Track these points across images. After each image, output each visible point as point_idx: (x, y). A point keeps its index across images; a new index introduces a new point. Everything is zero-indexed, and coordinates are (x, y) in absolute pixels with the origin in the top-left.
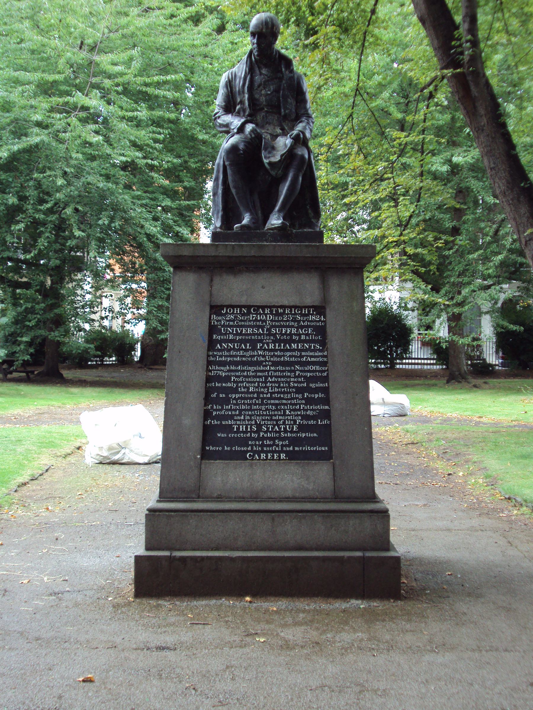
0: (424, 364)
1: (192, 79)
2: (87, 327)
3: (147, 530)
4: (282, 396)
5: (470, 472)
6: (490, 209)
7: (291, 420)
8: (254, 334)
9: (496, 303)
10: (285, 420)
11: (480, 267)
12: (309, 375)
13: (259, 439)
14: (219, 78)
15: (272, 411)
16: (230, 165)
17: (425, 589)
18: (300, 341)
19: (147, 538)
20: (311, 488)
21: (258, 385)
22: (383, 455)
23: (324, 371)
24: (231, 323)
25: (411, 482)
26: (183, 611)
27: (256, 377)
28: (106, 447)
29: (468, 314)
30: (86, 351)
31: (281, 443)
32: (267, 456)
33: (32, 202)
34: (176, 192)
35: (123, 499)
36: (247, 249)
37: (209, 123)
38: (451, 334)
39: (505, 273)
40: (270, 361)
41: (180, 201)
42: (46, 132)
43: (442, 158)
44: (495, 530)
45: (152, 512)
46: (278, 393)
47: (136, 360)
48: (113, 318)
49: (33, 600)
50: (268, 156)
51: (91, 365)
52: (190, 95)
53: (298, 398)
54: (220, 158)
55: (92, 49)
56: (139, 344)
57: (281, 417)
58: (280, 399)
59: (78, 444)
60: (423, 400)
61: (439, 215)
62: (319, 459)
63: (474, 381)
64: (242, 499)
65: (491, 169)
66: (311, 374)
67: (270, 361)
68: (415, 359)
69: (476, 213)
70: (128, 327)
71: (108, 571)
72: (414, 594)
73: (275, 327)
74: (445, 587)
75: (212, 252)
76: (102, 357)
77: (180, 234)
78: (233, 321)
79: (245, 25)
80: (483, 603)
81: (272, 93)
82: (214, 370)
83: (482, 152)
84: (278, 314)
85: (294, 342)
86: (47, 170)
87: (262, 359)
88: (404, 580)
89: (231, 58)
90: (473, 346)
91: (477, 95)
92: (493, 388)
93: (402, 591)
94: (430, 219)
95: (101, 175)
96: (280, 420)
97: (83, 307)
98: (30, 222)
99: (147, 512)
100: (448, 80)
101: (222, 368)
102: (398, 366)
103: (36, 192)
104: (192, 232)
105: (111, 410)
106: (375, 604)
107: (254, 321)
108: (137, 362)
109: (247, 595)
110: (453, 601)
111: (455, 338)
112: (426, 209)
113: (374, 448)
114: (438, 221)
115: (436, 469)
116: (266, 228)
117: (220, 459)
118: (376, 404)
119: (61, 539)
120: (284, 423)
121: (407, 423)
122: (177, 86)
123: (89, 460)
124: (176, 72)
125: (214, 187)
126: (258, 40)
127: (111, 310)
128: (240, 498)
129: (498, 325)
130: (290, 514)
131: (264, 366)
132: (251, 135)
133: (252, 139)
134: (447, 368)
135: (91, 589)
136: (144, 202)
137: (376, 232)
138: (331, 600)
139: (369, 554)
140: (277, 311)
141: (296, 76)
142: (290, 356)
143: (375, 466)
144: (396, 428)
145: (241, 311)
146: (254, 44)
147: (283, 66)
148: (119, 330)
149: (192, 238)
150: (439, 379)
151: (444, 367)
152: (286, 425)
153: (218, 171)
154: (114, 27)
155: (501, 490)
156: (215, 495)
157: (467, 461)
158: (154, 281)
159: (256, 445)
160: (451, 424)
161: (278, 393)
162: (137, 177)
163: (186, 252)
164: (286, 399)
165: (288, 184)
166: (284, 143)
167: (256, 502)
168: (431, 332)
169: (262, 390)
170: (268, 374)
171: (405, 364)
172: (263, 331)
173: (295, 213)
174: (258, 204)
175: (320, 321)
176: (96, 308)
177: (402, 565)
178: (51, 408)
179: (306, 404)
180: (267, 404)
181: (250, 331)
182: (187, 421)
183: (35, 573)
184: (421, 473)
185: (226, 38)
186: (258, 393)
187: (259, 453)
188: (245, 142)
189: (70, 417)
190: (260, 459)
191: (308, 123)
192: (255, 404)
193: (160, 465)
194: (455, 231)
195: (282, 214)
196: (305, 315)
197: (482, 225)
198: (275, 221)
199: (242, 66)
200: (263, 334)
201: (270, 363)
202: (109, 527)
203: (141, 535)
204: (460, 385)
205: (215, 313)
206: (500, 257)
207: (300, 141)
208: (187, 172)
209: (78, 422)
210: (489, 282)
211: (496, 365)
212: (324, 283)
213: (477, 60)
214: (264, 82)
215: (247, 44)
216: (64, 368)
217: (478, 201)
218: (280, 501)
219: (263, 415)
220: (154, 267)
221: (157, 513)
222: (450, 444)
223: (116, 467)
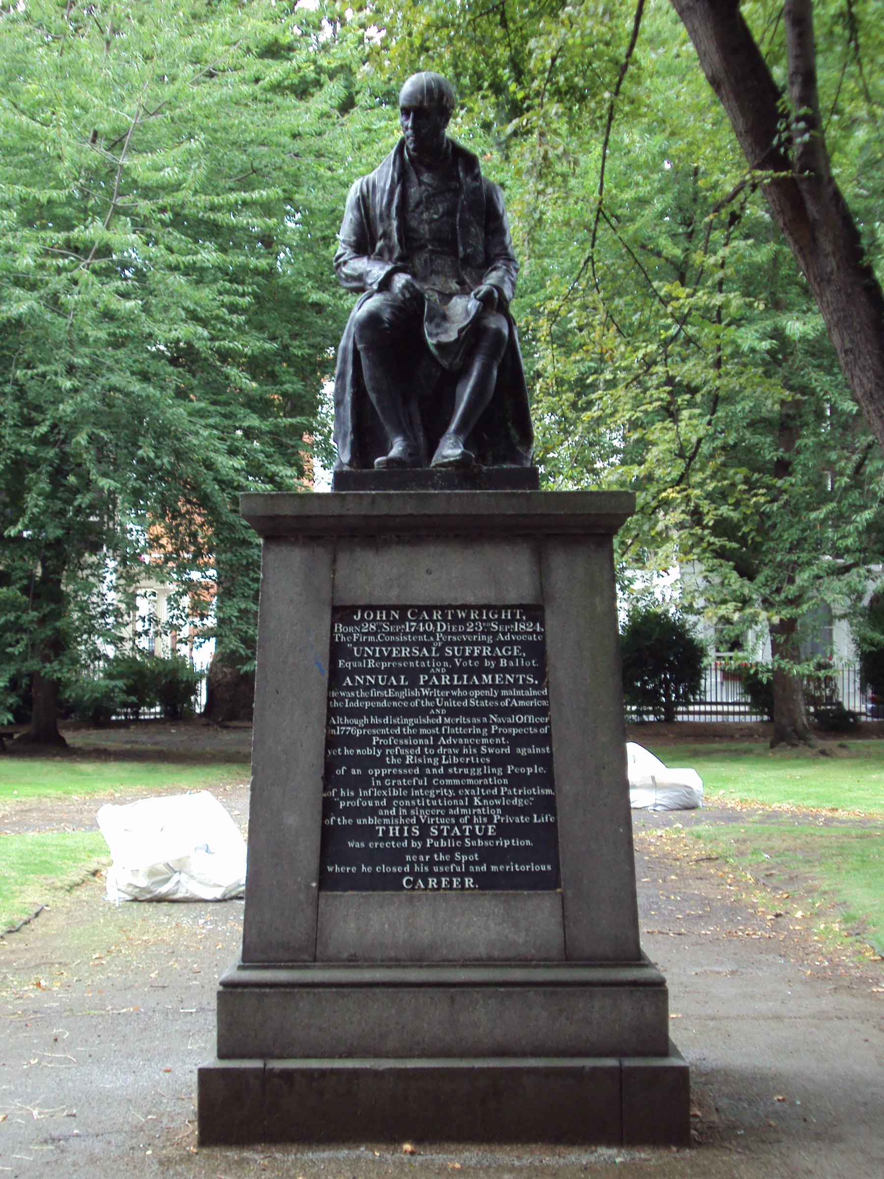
0: (728, 713)
1: (297, 197)
2: (110, 651)
3: (220, 1021)
4: (466, 771)
5: (816, 911)
6: (846, 425)
7: (483, 816)
8: (413, 659)
9: (860, 598)
10: (472, 816)
11: (830, 533)
12: (514, 731)
13: (424, 851)
14: (344, 191)
15: (448, 798)
16: (365, 348)
17: (735, 1128)
18: (498, 670)
19: (220, 1037)
20: (521, 941)
21: (422, 751)
22: (655, 881)
23: (543, 725)
24: (371, 639)
25: (708, 931)
26: (288, 1171)
27: (417, 736)
28: (144, 869)
29: (808, 620)
30: (108, 695)
31: (464, 858)
32: (439, 883)
33: (11, 422)
34: (269, 403)
35: (176, 965)
36: (399, 502)
37: (328, 275)
38: (777, 657)
39: (875, 543)
40: (443, 707)
41: (276, 418)
42: (36, 294)
43: (756, 331)
44: (864, 1018)
45: (229, 987)
46: (459, 765)
47: (198, 711)
48: (157, 634)
49: (13, 1152)
50: (435, 331)
51: (117, 721)
52: (291, 225)
53: (495, 775)
54: (348, 337)
55: (113, 146)
56: (204, 681)
57: (464, 811)
58: (462, 776)
59: (93, 866)
60: (726, 780)
61: (751, 438)
62: (535, 887)
63: (821, 744)
64: (396, 963)
65: (846, 352)
66: (519, 731)
67: (443, 707)
68: (711, 703)
69: (820, 434)
70: (184, 650)
71: (149, 1098)
72: (713, 1137)
73: (452, 644)
74: (772, 1123)
75: (336, 509)
76: (136, 707)
77: (277, 479)
78: (375, 634)
79: (389, 97)
80: (842, 1152)
81: (441, 217)
82: (340, 725)
83: (828, 322)
84: (456, 621)
85: (487, 671)
86: (38, 364)
87: (428, 703)
88: (695, 1111)
89: (368, 157)
90: (819, 679)
91: (817, 216)
92: (857, 756)
93: (693, 1132)
94: (736, 444)
95: (133, 373)
96: (463, 816)
97: (103, 614)
98: (10, 458)
99: (221, 988)
100: (764, 191)
101: (356, 722)
102: (679, 718)
103: (16, 405)
104: (301, 473)
105: (154, 802)
106: (642, 1154)
107: (412, 634)
108: (201, 715)
109: (404, 1139)
110: (788, 1148)
111: (785, 664)
112: (728, 427)
113: (638, 869)
114: (749, 450)
115: (754, 906)
116: (433, 464)
117: (352, 889)
118: (641, 787)
119: (63, 1040)
120: (470, 821)
121: (698, 822)
122: (266, 209)
123: (115, 895)
124: (268, 186)
125: (336, 390)
126: (414, 122)
127: (153, 619)
128: (390, 959)
129: (864, 639)
130: (484, 989)
131: (431, 716)
132: (403, 295)
133: (405, 301)
134: (771, 720)
135: (119, 1131)
136: (211, 421)
137: (637, 471)
138: (561, 1149)
139: (629, 1063)
140: (455, 615)
141: (484, 186)
142: (480, 698)
143: (640, 901)
144: (678, 831)
145: (388, 615)
146: (407, 128)
147: (460, 168)
148: (168, 656)
149: (303, 486)
150: (756, 741)
151: (766, 718)
152: (473, 825)
153: (344, 361)
154: (155, 105)
155: (874, 943)
156: (345, 955)
157: (810, 891)
158: (231, 566)
159: (419, 863)
160: (780, 824)
161: (459, 765)
162: (198, 377)
163: (287, 509)
164: (474, 778)
165: (472, 382)
166: (463, 308)
167: (421, 967)
168: (740, 654)
169: (430, 760)
170: (440, 730)
171: (694, 713)
172: (430, 651)
173: (485, 436)
174: (418, 420)
175: (534, 632)
176: (126, 617)
177: (691, 1083)
178: (44, 800)
179: (510, 786)
180: (438, 787)
181: (405, 652)
182: (291, 820)
183: (17, 1102)
184: (726, 914)
185: (357, 119)
186: (422, 767)
187: (425, 877)
188: (392, 306)
189: (78, 817)
190: (426, 888)
191: (508, 271)
192: (417, 787)
193: (243, 902)
194: (782, 468)
195: (461, 438)
196: (506, 622)
197: (833, 456)
198: (450, 450)
199: (385, 169)
200: (430, 658)
201: (444, 711)
202: (150, 1018)
203: (209, 1031)
204: (795, 751)
205: (341, 621)
206: (868, 515)
207: (494, 303)
208: (289, 366)
209: (94, 825)
210: (848, 560)
211: (861, 714)
212: (542, 571)
213: (816, 155)
214: (426, 198)
215: (394, 130)
216: (67, 728)
217: (823, 410)
218: (464, 966)
219: (432, 807)
220: (228, 540)
221: (239, 990)
222: (779, 860)
223: (164, 906)
